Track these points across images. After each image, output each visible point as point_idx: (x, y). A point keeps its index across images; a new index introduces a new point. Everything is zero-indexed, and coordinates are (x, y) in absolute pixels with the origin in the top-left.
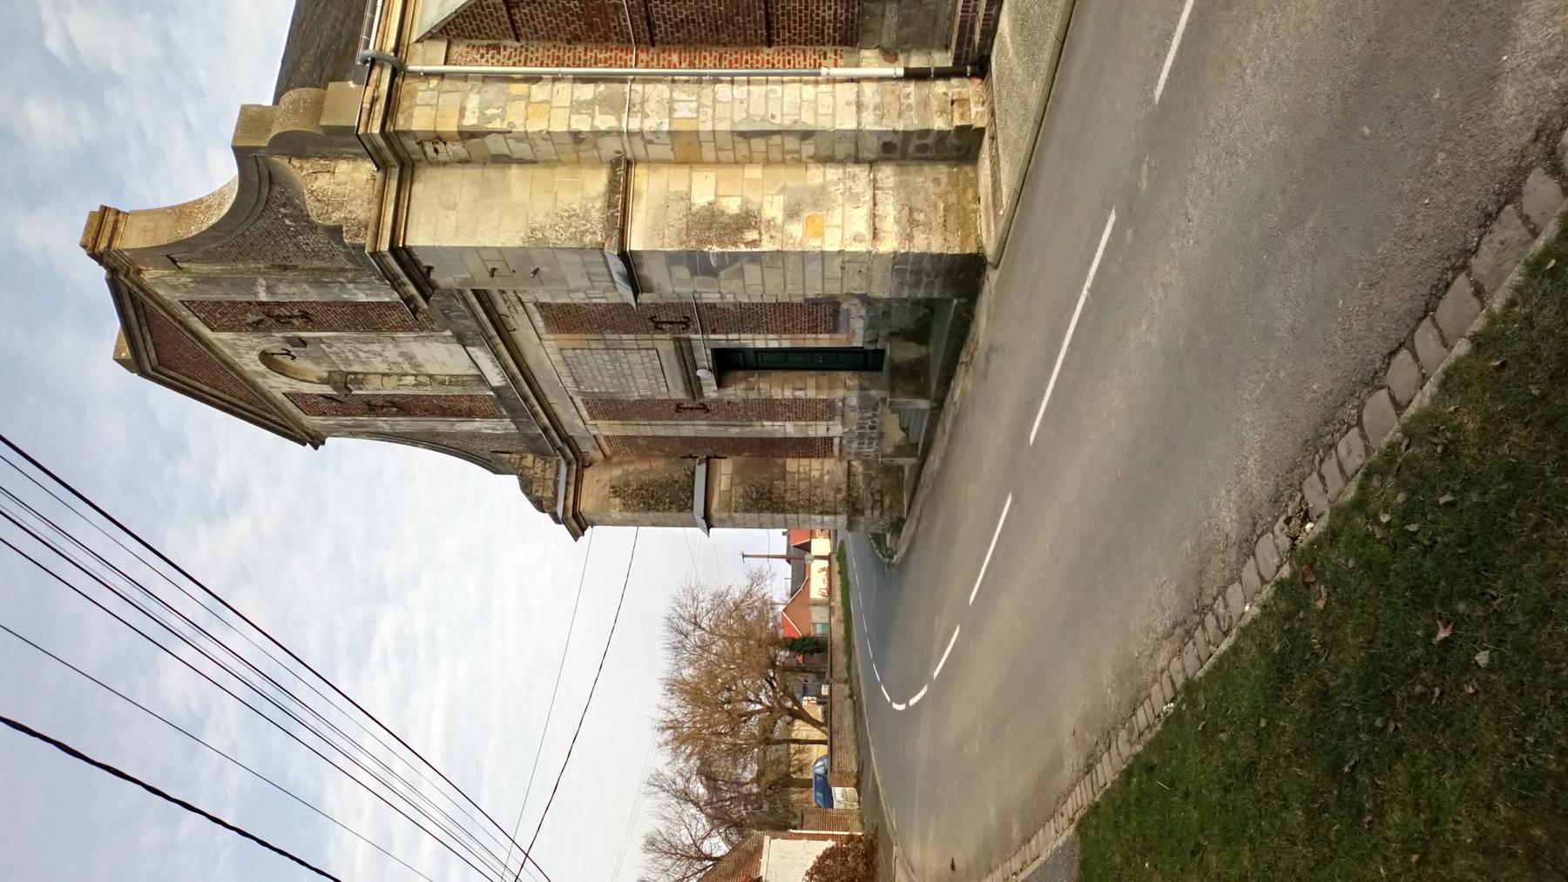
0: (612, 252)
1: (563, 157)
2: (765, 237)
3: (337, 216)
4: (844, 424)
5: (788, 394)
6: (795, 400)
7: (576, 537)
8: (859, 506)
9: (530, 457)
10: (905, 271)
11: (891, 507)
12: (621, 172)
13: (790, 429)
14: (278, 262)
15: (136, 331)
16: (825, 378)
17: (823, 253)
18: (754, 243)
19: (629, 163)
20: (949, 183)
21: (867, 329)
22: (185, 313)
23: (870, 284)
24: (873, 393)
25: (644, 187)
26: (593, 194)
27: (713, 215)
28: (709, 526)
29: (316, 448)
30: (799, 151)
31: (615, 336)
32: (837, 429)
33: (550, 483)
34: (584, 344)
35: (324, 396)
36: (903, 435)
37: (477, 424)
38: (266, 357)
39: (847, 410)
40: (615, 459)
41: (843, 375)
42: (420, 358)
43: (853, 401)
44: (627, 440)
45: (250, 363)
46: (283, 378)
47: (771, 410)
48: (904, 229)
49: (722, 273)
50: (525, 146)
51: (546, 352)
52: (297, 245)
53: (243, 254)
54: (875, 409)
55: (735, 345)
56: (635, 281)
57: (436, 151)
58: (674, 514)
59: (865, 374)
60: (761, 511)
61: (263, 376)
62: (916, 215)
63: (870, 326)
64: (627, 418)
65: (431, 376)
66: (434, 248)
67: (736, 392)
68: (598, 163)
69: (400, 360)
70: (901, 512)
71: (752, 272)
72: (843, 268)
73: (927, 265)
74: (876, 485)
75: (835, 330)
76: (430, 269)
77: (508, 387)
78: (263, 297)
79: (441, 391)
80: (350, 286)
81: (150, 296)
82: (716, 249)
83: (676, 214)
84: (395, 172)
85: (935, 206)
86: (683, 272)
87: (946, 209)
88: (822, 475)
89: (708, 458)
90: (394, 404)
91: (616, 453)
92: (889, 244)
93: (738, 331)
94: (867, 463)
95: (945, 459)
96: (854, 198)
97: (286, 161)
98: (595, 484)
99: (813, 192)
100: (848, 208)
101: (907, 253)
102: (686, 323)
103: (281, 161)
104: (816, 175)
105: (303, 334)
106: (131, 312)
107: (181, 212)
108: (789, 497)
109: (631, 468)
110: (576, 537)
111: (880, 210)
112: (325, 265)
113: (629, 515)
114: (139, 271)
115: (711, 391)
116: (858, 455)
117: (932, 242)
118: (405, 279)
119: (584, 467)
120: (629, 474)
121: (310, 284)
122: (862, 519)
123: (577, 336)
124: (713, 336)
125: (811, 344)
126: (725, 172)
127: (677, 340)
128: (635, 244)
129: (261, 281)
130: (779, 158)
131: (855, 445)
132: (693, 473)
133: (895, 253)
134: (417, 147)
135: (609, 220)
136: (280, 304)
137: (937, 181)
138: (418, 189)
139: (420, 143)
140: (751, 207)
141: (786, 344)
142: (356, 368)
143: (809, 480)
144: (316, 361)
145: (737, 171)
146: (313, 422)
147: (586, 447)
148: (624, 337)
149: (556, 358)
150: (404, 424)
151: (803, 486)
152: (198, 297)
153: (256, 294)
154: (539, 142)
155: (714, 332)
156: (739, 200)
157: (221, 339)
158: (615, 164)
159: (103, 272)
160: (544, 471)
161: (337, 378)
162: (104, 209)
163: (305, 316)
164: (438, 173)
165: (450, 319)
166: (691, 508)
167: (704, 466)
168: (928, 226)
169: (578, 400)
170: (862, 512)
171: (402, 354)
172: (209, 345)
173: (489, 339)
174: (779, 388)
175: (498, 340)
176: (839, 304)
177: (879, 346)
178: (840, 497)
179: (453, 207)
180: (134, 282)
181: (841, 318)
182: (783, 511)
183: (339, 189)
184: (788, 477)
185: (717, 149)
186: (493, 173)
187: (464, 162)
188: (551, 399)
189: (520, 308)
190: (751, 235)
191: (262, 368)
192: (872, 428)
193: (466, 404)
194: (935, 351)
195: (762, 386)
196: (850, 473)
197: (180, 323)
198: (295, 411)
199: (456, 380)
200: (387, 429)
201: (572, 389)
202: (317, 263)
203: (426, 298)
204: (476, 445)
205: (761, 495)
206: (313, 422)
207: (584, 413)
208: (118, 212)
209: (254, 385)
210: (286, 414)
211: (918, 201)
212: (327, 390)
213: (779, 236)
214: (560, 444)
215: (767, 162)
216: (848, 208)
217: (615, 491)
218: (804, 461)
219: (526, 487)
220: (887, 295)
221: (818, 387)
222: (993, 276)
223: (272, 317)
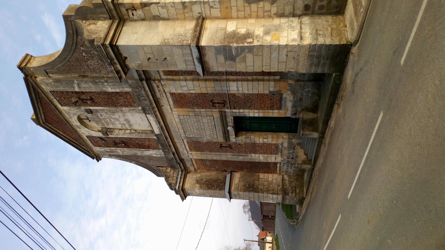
0: (194, 45)
1: (179, 16)
2: (255, 41)
3: (93, 37)
4: (282, 156)
5: (261, 141)
6: (264, 144)
7: (183, 200)
8: (286, 192)
9: (169, 169)
10: (314, 55)
11: (299, 193)
12: (200, 21)
13: (261, 158)
14: (82, 74)
15: (36, 105)
16: (275, 135)
17: (279, 46)
18: (251, 43)
19: (203, 19)
20: (332, 22)
21: (293, 108)
22: (52, 97)
23: (298, 65)
24: (294, 141)
25: (209, 26)
26: (189, 28)
27: (235, 34)
28: (231, 198)
29: (98, 161)
30: (270, 11)
31: (198, 110)
32: (279, 159)
33: (175, 178)
34: (187, 114)
35: (99, 137)
36: (305, 157)
37: (151, 152)
38: (80, 119)
39: (283, 149)
40: (199, 171)
41: (282, 134)
42: (132, 122)
43: (286, 145)
44: (202, 161)
45: (75, 122)
46: (86, 129)
47: (254, 148)
48: (314, 36)
49: (237, 59)
50: (165, 11)
51: (174, 115)
52: (88, 66)
53: (69, 71)
54: (294, 149)
55: (242, 115)
56: (201, 60)
57: (133, 14)
58: (218, 191)
59: (290, 134)
60: (250, 191)
61: (79, 128)
62: (319, 32)
63: (294, 106)
64: (202, 151)
65: (135, 130)
66: (127, 46)
67: (242, 139)
68: (192, 18)
69: (125, 122)
70: (303, 194)
71: (249, 57)
72: (287, 56)
73: (323, 52)
74: (293, 184)
75: (280, 108)
76: (126, 58)
77: (161, 134)
78: (77, 89)
79: (138, 136)
80: (106, 84)
81: (39, 88)
82: (235, 45)
83: (220, 35)
84: (117, 22)
85: (327, 29)
86: (221, 58)
87: (332, 30)
88: (273, 180)
89: (231, 172)
90: (123, 142)
91: (199, 168)
92: (308, 41)
93: (243, 108)
94: (289, 176)
95: (326, 158)
96: (293, 28)
97: (81, 21)
98: (190, 182)
99: (275, 26)
100: (290, 31)
101: (315, 45)
102: (223, 104)
103: (79, 21)
104: (277, 21)
105: (91, 108)
106: (33, 95)
107: (51, 55)
108: (260, 187)
109: (204, 174)
110: (183, 200)
111: (303, 31)
112: (97, 75)
113: (202, 191)
114: (36, 77)
115: (233, 139)
116: (287, 172)
117: (326, 40)
118: (116, 61)
119: (187, 173)
120: (203, 176)
121: (92, 82)
122: (288, 197)
123: (185, 110)
124: (234, 111)
125: (270, 115)
126: (240, 21)
127: (221, 112)
128: (203, 42)
129: (76, 82)
130: (262, 15)
131: (285, 167)
132: (226, 177)
133: (310, 45)
134: (125, 12)
135: (194, 37)
136: (83, 93)
137: (327, 21)
138: (125, 28)
139: (127, 10)
140: (250, 31)
141: (261, 115)
142: (111, 126)
143: (268, 181)
144: (97, 123)
145: (245, 21)
146: (97, 149)
147: (188, 164)
148: (202, 110)
149: (177, 120)
150: (127, 151)
151: (266, 183)
152: (55, 89)
153: (74, 88)
154: (170, 8)
155: (234, 108)
156: (245, 30)
157: (64, 109)
158: (198, 19)
159: (22, 75)
160: (173, 174)
161: (104, 130)
162: (27, 55)
163: (91, 99)
164: (133, 24)
165: (140, 101)
166: (224, 189)
167: (230, 174)
168: (324, 35)
169: (185, 141)
170: (288, 194)
171: (126, 120)
172: (60, 112)
173: (155, 112)
174: (259, 139)
175: (156, 109)
176: (282, 94)
177: (297, 116)
178: (279, 188)
179: (137, 33)
180: (33, 81)
181: (283, 102)
182: (258, 192)
183: (97, 29)
184: (260, 180)
185: (238, 11)
186: (153, 23)
187: (143, 20)
188: (176, 141)
189: (164, 95)
190: (251, 40)
191: (79, 124)
192: (292, 158)
193: (147, 143)
194: (320, 115)
195: (252, 137)
196: (283, 180)
197: (50, 101)
198: (91, 144)
199: (144, 132)
200: (121, 154)
201: (183, 136)
202: (95, 75)
203: (125, 74)
204: (151, 163)
205: (250, 186)
206: (97, 149)
207: (187, 148)
208: (32, 56)
209: (76, 132)
210: (87, 146)
211: (319, 27)
212: (100, 135)
213: (261, 40)
214: (179, 161)
215: (257, 17)
216: (290, 31)
217: (198, 182)
218: (266, 175)
219: (167, 180)
220: (304, 72)
221: (272, 138)
222: (354, 50)
223: (81, 99)
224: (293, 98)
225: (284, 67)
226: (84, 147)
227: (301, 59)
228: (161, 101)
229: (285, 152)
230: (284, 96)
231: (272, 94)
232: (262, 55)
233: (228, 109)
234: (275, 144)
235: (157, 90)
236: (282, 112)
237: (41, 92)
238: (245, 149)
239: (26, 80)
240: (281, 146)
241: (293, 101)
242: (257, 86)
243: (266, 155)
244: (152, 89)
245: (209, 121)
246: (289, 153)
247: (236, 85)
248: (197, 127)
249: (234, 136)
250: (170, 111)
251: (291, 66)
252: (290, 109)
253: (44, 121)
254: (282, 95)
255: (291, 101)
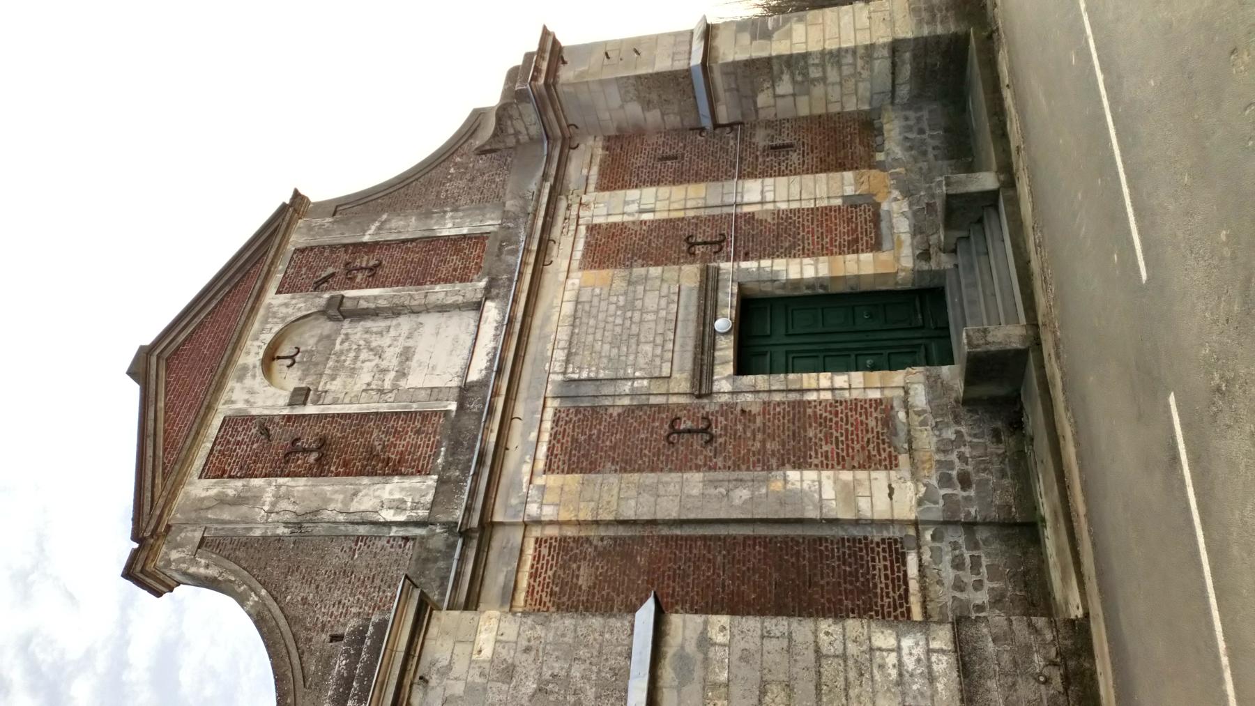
4: (915, 477)
21: (914, 235)
31: (642, 271)
39: (916, 420)
49: (775, 35)
72: (870, 18)
75: (876, 246)
86: (745, 38)
93: (772, 255)
95: (1022, 112)
102: (718, 245)
115: (724, 378)
124: (744, 265)
149: (568, 308)
155: (747, 257)
175: (532, 259)
176: (879, 205)
181: (884, 225)
189: (573, 227)
220: (910, 35)
224: (910, 205)
225: (868, 37)
226: (159, 481)
227: (899, 16)
228: (555, 247)
229: (926, 440)
230: (885, 206)
231: (852, 203)
232: (823, 24)
233: (728, 260)
234: (878, 402)
235: (560, 219)
236: (885, 256)
237: (268, 262)
238: (763, 442)
239: (283, 209)
240: (902, 415)
241: (909, 215)
242: (811, 184)
243: (846, 476)
244: (551, 211)
245: (663, 302)
246: (944, 447)
247: (760, 188)
248: (618, 329)
249: (730, 369)
250: (562, 277)
251: (881, 32)
252: (906, 238)
253: (166, 354)
254: (877, 206)
255: (903, 213)
